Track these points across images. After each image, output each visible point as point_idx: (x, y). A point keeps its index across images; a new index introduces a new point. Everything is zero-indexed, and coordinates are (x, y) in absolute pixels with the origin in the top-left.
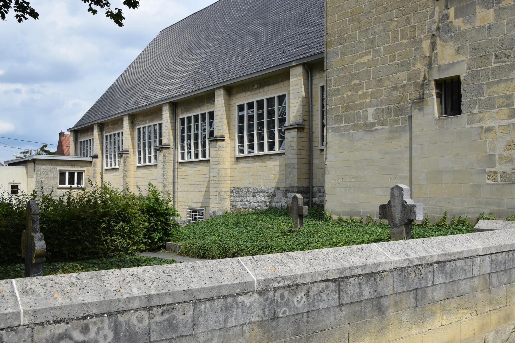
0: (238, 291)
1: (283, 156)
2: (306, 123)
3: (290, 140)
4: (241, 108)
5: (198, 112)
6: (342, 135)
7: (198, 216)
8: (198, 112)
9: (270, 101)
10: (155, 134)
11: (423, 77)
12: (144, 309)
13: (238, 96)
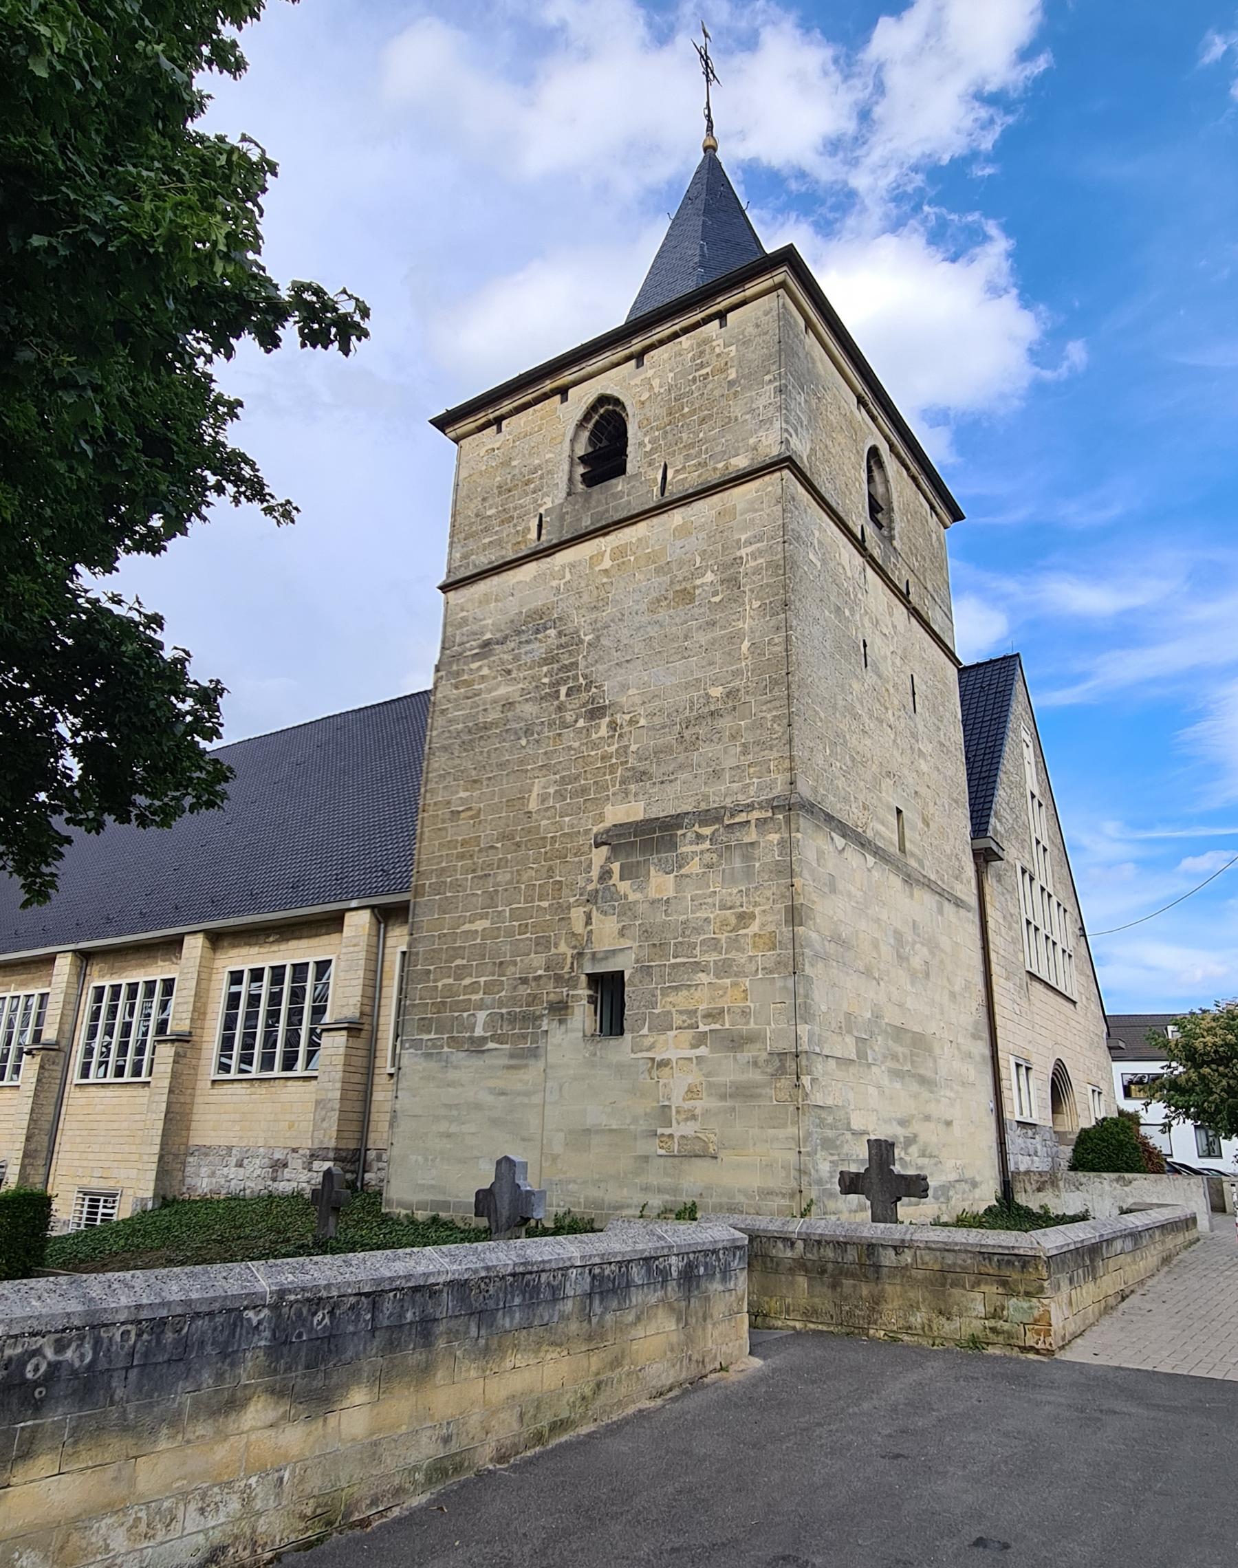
0: (245, 1303)
1: (314, 1082)
2: (366, 1020)
3: (329, 1052)
4: (236, 977)
5: (140, 976)
6: (428, 1056)
7: (101, 1210)
8: (140, 976)
9: (300, 969)
10: (26, 1016)
11: (569, 965)
12: (132, 1323)
13: (234, 952)
